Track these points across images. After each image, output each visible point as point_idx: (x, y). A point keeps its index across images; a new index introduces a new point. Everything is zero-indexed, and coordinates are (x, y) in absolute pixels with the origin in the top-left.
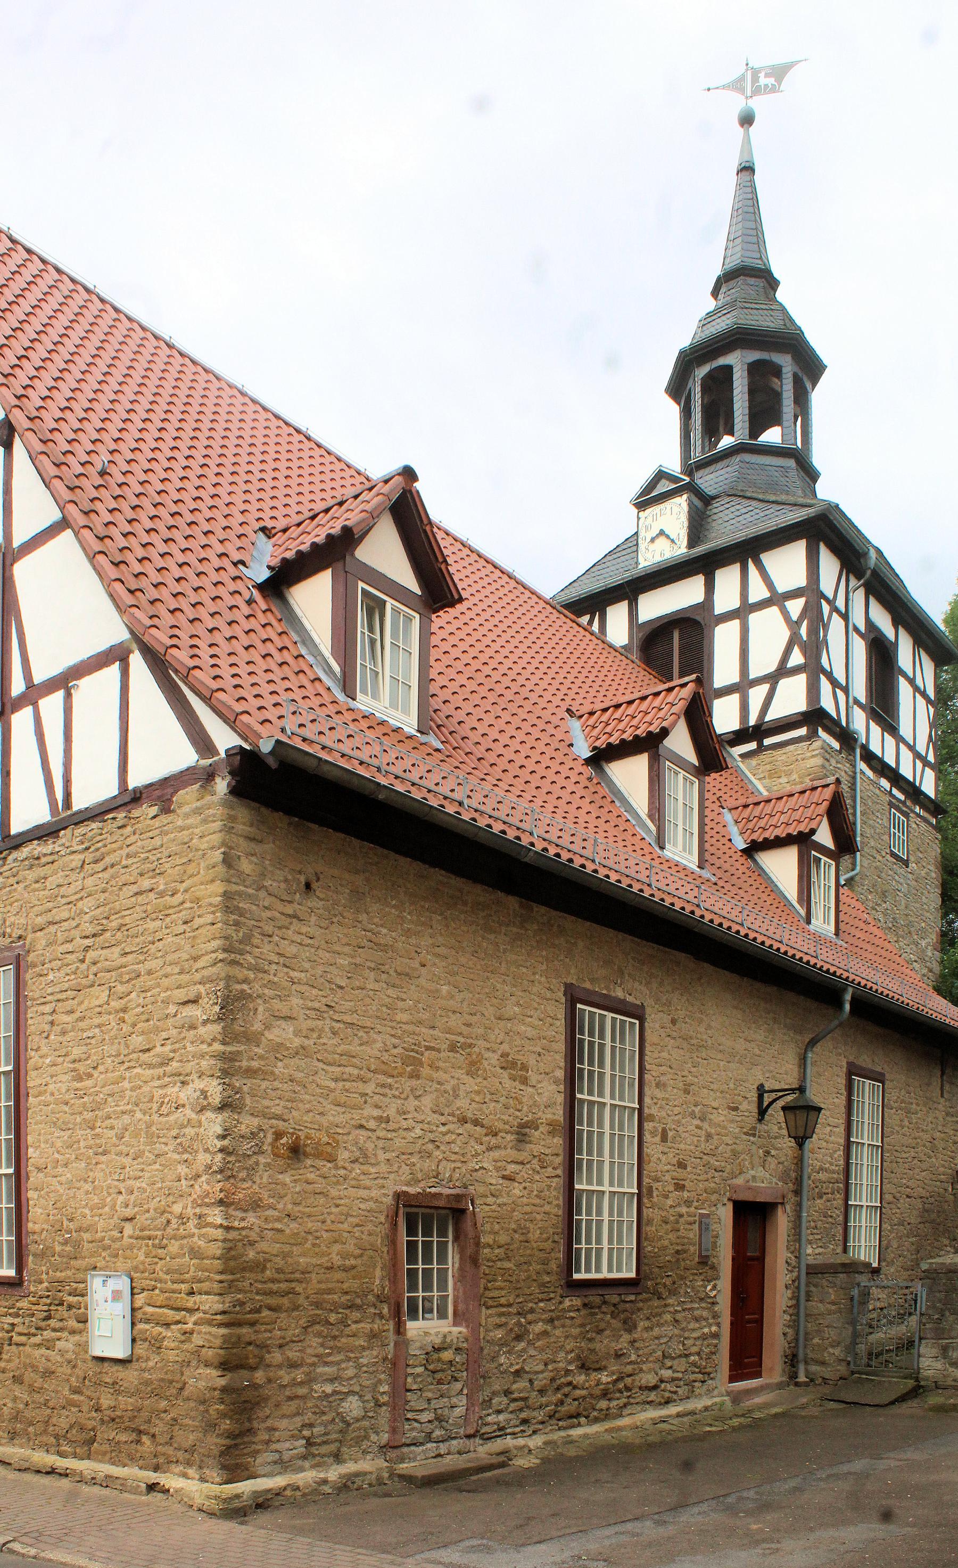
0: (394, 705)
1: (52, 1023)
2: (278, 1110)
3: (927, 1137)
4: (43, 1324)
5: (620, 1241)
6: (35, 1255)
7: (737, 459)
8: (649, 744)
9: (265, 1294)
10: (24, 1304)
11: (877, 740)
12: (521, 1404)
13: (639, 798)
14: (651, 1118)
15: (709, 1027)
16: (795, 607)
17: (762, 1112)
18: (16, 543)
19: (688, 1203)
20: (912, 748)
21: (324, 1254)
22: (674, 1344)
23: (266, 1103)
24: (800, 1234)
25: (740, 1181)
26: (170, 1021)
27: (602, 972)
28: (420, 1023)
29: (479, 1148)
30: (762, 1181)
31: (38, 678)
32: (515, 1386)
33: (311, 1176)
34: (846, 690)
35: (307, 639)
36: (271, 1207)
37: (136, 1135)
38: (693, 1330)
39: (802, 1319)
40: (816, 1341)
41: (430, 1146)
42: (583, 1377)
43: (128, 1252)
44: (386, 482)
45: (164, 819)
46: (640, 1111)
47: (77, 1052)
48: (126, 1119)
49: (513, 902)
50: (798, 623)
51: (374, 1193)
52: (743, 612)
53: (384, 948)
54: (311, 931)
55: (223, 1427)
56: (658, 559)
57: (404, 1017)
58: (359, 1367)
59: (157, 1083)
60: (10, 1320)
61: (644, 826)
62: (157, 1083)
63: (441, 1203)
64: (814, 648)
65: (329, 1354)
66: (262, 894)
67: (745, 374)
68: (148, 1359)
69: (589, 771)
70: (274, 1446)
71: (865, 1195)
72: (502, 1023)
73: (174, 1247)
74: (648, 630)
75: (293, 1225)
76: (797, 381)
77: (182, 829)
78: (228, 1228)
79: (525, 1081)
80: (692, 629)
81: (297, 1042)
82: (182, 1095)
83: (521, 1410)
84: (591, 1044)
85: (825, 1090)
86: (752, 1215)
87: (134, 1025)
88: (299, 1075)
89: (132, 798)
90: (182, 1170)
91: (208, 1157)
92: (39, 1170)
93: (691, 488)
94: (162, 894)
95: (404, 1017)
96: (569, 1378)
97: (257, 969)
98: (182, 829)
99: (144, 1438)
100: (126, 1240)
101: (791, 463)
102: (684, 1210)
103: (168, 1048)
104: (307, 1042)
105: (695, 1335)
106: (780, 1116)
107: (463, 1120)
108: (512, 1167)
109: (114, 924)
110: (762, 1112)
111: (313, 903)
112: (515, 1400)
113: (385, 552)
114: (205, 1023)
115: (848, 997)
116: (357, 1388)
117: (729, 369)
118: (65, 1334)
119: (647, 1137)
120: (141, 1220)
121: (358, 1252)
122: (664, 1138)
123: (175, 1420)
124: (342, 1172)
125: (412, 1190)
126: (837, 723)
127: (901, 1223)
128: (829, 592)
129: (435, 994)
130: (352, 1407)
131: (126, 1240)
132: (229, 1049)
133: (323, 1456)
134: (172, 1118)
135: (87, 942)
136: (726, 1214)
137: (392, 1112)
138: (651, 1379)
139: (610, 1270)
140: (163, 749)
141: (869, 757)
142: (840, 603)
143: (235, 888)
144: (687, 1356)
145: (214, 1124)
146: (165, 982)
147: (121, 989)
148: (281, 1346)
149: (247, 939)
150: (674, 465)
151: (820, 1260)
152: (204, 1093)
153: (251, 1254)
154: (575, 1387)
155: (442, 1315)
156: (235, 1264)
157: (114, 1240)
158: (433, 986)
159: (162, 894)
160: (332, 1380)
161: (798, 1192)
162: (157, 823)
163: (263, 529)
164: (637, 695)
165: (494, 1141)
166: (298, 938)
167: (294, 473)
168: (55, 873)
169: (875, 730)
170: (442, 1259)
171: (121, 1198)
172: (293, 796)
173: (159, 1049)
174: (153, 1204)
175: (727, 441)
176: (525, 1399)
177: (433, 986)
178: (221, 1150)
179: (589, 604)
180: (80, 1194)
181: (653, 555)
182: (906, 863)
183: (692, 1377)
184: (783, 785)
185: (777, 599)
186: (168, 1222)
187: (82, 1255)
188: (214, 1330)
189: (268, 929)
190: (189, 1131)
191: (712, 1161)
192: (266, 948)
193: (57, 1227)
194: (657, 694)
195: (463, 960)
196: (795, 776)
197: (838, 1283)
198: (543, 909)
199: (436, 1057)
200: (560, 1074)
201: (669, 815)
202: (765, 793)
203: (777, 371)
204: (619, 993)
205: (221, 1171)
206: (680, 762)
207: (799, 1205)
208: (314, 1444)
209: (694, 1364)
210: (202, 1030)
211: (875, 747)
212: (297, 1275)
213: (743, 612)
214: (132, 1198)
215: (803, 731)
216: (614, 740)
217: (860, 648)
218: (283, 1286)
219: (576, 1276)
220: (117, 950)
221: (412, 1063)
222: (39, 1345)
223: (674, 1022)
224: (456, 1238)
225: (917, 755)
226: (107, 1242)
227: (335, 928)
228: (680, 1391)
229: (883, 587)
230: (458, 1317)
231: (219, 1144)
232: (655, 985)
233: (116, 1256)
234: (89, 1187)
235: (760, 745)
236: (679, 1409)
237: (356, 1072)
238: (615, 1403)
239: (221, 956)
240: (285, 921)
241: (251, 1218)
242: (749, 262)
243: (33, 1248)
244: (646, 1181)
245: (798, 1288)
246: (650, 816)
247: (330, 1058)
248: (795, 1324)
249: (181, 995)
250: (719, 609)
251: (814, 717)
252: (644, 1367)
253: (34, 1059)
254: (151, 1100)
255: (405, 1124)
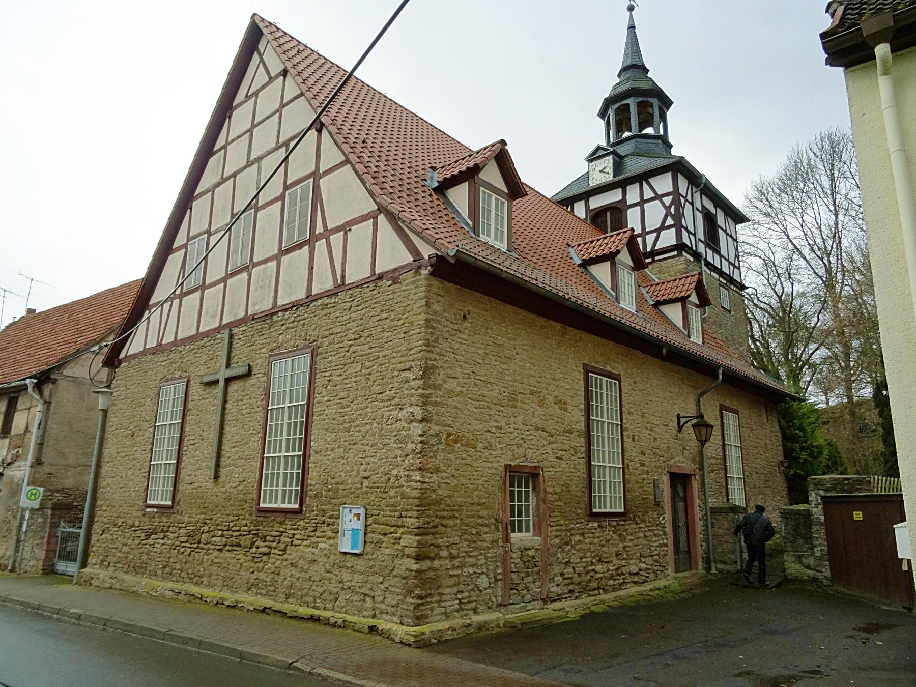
0: (496, 239)
1: (329, 381)
2: (449, 423)
3: (763, 442)
4: (312, 534)
5: (615, 493)
6: (310, 497)
7: (634, 141)
8: (611, 257)
9: (440, 518)
10: (302, 523)
11: (710, 256)
12: (569, 581)
13: (607, 283)
14: (627, 429)
15: (652, 385)
16: (667, 200)
17: (680, 428)
18: (321, 171)
19: (647, 473)
20: (727, 260)
21: (469, 496)
22: (645, 549)
23: (443, 419)
24: (704, 491)
25: (671, 462)
26: (395, 379)
27: (600, 359)
28: (516, 381)
29: (545, 443)
30: (684, 464)
31: (330, 226)
32: (565, 571)
33: (464, 456)
34: (694, 235)
35: (455, 211)
36: (445, 471)
37: (373, 435)
38: (655, 542)
39: (711, 538)
40: (719, 550)
41: (521, 441)
42: (600, 567)
43: (365, 495)
44: (493, 146)
45: (395, 286)
46: (621, 425)
47: (342, 395)
48: (368, 427)
49: (558, 326)
50: (670, 207)
51: (494, 465)
52: (642, 203)
53: (500, 346)
54: (466, 337)
55: (416, 592)
56: (599, 182)
57: (509, 378)
58: (486, 558)
59: (386, 409)
60: (293, 532)
61: (609, 293)
62: (386, 409)
63: (527, 470)
64: (678, 217)
65: (471, 551)
66: (443, 320)
67: (637, 105)
68: (373, 554)
69: (581, 269)
70: (443, 604)
71: (735, 471)
72: (554, 382)
73: (392, 492)
74: (594, 212)
75: (455, 481)
76: (660, 109)
77: (405, 291)
78: (423, 482)
79: (566, 410)
80: (618, 211)
81: (459, 389)
82: (400, 415)
83: (569, 584)
84: (596, 392)
85: (711, 417)
86: (679, 480)
87: (374, 381)
88: (459, 405)
89: (198, 336)
90: (399, 452)
91: (414, 446)
92: (317, 453)
93: (614, 153)
94: (392, 320)
95: (509, 378)
96: (593, 567)
97: (441, 354)
98: (405, 291)
99: (368, 599)
100: (364, 489)
101: (660, 141)
102: (645, 476)
103: (393, 392)
104: (463, 389)
105: (655, 544)
106: (691, 430)
107: (538, 429)
108: (561, 453)
109: (366, 334)
110: (680, 428)
111: (467, 324)
112: (566, 579)
113: (492, 175)
114: (414, 379)
115: (721, 372)
116: (485, 570)
117: (628, 105)
118: (324, 539)
119: (625, 439)
120: (374, 478)
121: (486, 495)
122: (634, 440)
123: (387, 588)
124: (479, 454)
125: (513, 463)
126: (691, 248)
127: (755, 487)
128: (683, 193)
129: (522, 367)
130: (483, 581)
131: (364, 489)
132: (426, 392)
133: (467, 610)
134: (394, 426)
135: (351, 343)
136: (665, 479)
137: (503, 424)
138: (634, 569)
139: (611, 508)
140: (393, 254)
141: (708, 264)
142: (689, 198)
143: (431, 317)
144: (652, 556)
145: (417, 429)
146: (393, 361)
147: (368, 364)
148: (447, 546)
149: (436, 341)
150: (603, 144)
151: (716, 505)
152: (412, 414)
153: (434, 496)
154: (596, 572)
155: (528, 530)
156: (424, 503)
157: (357, 489)
158: (522, 364)
159: (392, 320)
160: (472, 566)
161: (701, 469)
162: (391, 288)
163: (431, 167)
164: (590, 240)
165: (552, 439)
166: (459, 340)
167: (441, 146)
168: (335, 311)
169: (710, 252)
170: (527, 500)
171: (362, 467)
172: (461, 275)
173: (388, 393)
174: (381, 470)
175: (627, 134)
176: (571, 578)
177: (522, 364)
178: (421, 442)
179: (567, 202)
180: (339, 465)
181: (598, 179)
182: (730, 311)
183: (656, 568)
184: (666, 277)
185: (658, 197)
186: (389, 479)
187: (337, 496)
188: (413, 537)
189: (446, 336)
190: (404, 433)
191: (658, 451)
192: (444, 345)
193: (325, 482)
194: (598, 240)
195: (536, 352)
196: (672, 273)
197: (730, 518)
198: (572, 329)
199: (526, 399)
200: (582, 407)
201: (621, 288)
202: (657, 281)
203: (651, 106)
204: (608, 368)
205: (420, 453)
206: (625, 265)
207: (703, 476)
208: (464, 603)
209: (656, 561)
210: (412, 383)
211: (710, 259)
212: (457, 508)
213: (642, 203)
214: (369, 467)
215: (675, 253)
216: (593, 255)
217: (699, 217)
218: (450, 513)
219: (594, 510)
220: (367, 346)
221: (513, 400)
222: (309, 546)
223: (635, 382)
224: (534, 489)
225: (730, 263)
226: (353, 490)
227: (477, 336)
228: (651, 576)
229: (709, 191)
230: (538, 530)
231: (420, 439)
232: (625, 364)
233: (358, 497)
234: (344, 461)
235: (653, 259)
236: (652, 586)
237: (486, 404)
238: (617, 582)
239: (424, 348)
240: (453, 332)
241: (434, 477)
242: (635, 63)
243: (310, 493)
244: (626, 461)
245: (706, 520)
246: (612, 288)
247: (474, 397)
248: (707, 540)
249: (401, 366)
250: (629, 202)
251: (680, 247)
252: (631, 562)
253: (318, 398)
254: (382, 417)
255: (509, 430)
